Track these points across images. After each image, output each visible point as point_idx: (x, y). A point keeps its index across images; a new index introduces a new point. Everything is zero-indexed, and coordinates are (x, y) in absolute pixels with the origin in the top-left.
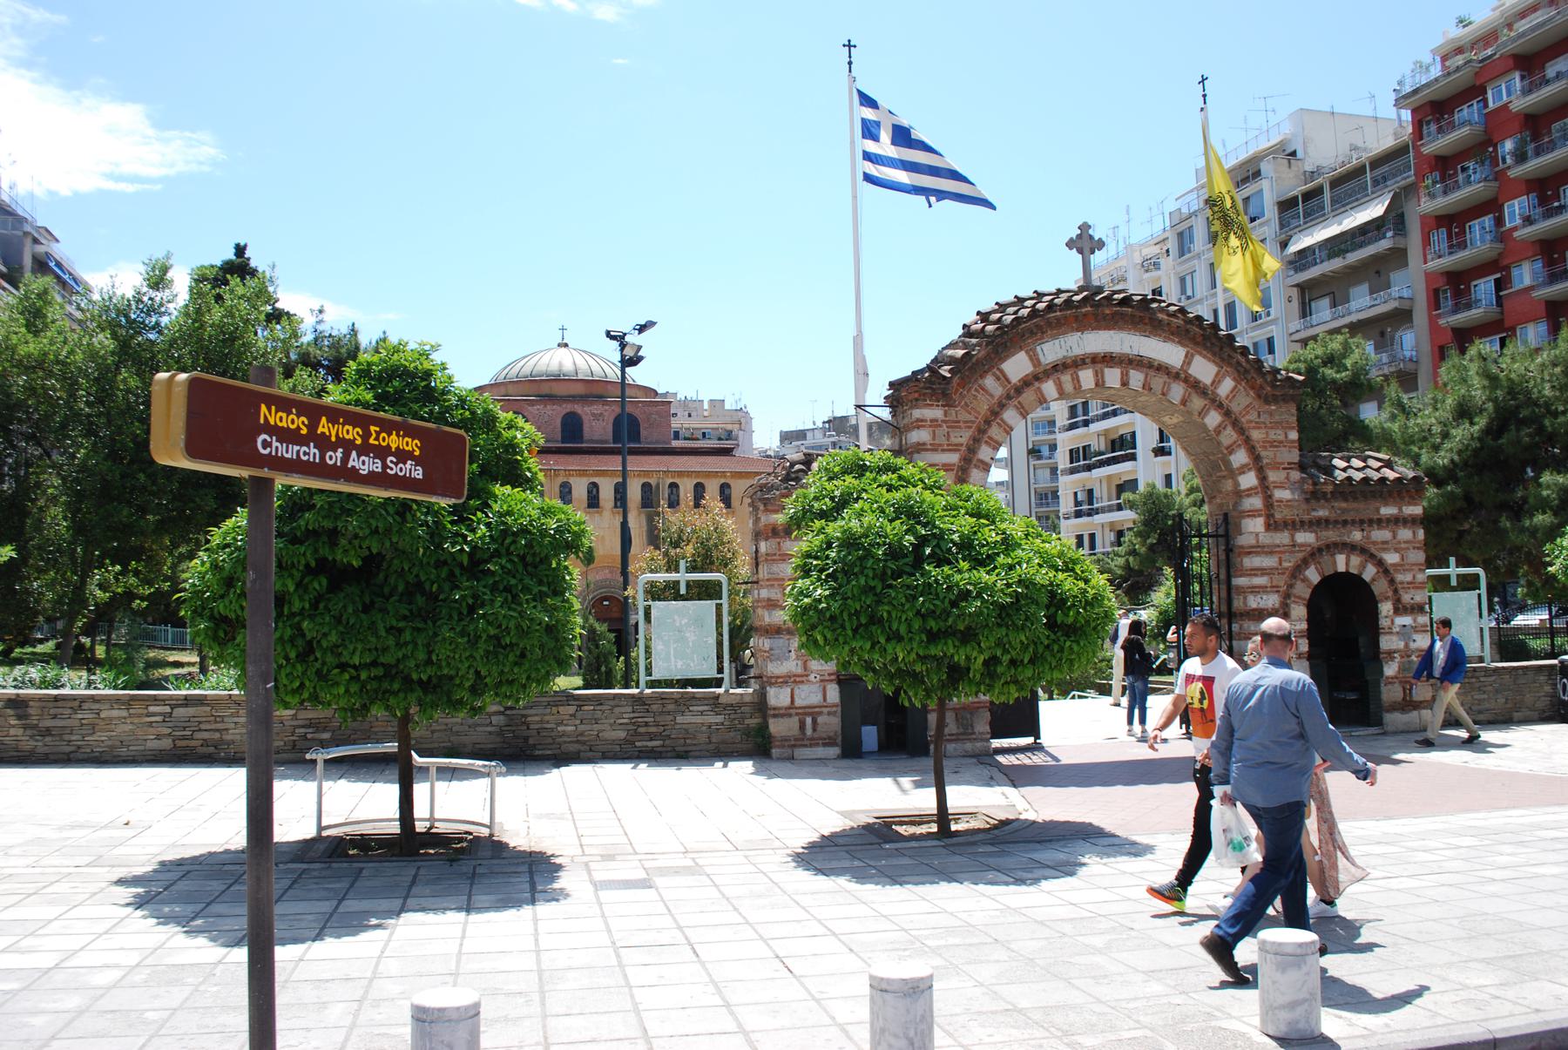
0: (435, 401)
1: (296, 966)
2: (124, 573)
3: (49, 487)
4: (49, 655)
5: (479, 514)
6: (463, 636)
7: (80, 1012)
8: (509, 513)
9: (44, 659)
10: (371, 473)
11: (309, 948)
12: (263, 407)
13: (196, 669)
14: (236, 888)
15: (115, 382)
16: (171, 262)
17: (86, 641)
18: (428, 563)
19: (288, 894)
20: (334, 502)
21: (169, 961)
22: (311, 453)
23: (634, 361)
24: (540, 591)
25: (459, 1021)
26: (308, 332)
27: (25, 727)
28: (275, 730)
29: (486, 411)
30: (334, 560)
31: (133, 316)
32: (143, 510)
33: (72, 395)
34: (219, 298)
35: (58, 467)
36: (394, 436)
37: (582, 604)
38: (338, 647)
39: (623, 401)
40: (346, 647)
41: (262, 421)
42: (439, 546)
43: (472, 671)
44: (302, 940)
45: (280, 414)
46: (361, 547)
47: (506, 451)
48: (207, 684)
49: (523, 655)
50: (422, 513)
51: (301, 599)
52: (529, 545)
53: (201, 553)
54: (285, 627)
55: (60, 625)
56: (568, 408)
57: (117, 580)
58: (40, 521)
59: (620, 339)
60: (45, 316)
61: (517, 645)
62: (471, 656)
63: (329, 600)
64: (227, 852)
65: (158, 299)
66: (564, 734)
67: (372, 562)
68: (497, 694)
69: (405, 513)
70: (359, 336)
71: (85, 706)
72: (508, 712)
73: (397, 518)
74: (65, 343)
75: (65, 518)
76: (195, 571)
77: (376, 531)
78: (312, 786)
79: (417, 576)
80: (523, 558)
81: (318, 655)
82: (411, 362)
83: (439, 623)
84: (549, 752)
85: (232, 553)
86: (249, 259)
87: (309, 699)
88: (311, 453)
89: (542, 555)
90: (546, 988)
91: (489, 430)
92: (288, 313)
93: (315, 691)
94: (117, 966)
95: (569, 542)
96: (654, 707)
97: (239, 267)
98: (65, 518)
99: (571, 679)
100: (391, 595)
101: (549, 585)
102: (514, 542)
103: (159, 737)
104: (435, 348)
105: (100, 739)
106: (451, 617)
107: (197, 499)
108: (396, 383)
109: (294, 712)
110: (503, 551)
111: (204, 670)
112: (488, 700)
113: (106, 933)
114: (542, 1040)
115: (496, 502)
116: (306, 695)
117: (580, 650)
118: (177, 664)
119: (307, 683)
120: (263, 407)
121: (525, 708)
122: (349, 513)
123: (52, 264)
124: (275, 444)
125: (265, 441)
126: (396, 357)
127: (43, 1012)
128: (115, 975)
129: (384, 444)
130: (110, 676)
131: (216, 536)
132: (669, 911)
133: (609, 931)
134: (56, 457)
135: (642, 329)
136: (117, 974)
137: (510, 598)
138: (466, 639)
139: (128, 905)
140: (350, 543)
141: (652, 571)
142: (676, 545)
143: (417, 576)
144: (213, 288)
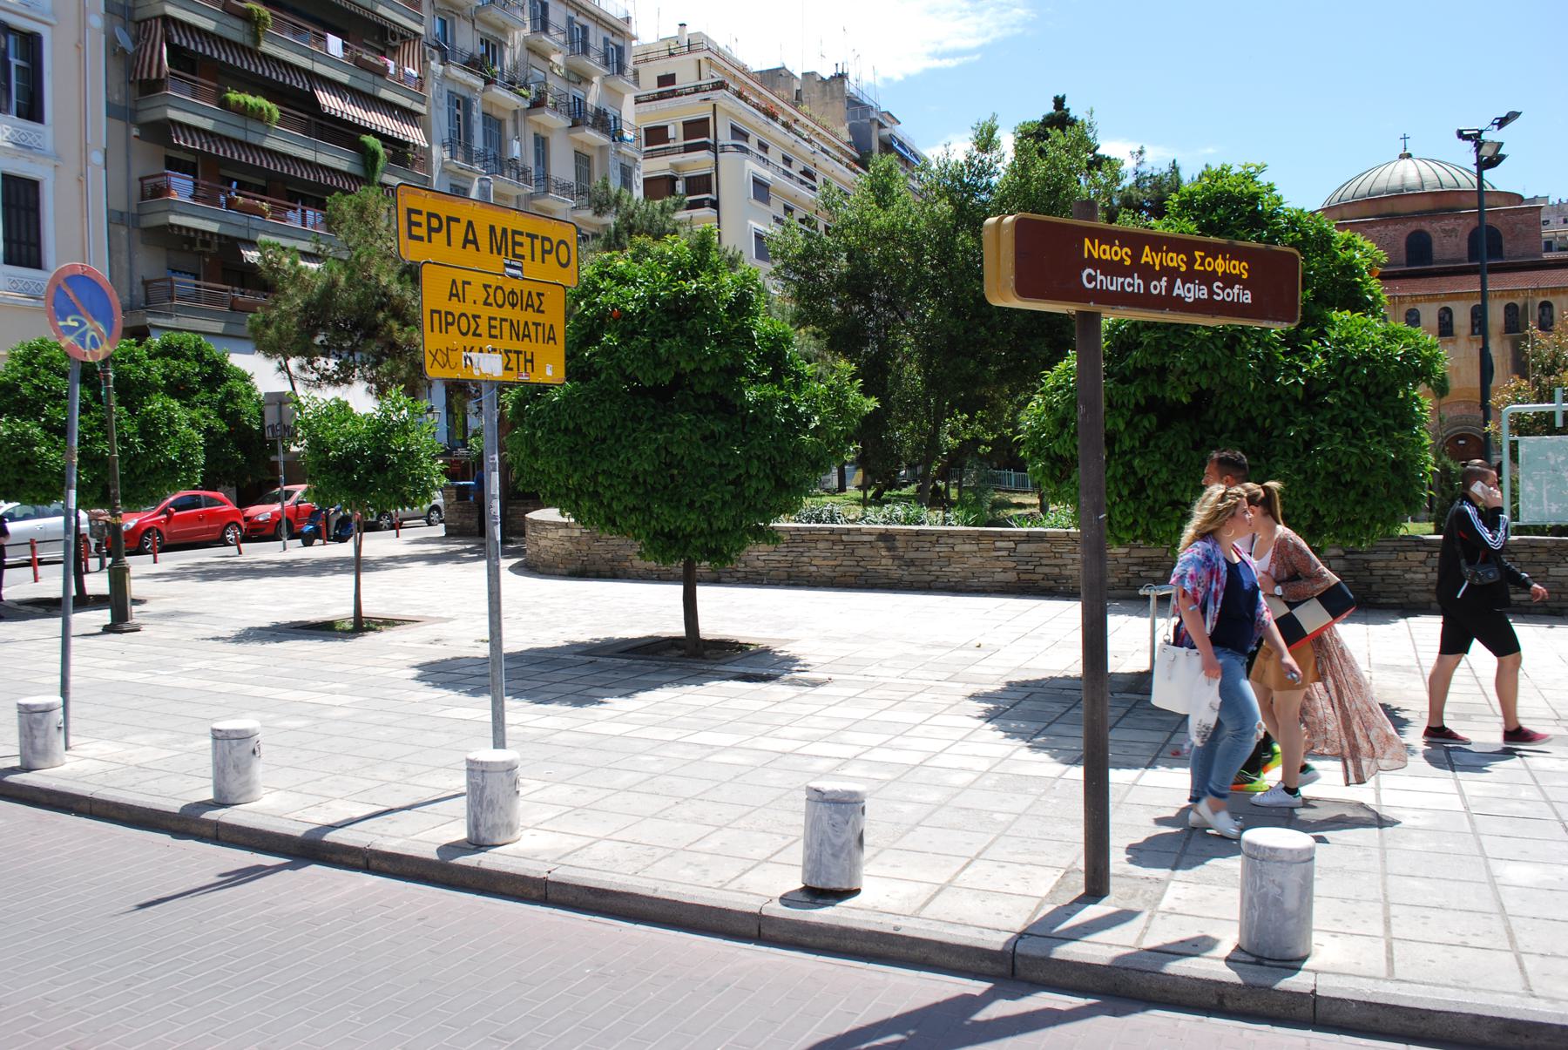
0: (1264, 226)
1: (1129, 790)
2: (971, 420)
3: (904, 346)
4: (912, 497)
5: (1315, 343)
6: (1299, 474)
7: (941, 806)
8: (1349, 340)
9: (907, 499)
10: (1197, 300)
11: (1142, 774)
12: (1087, 242)
13: (1036, 510)
14: (1075, 711)
15: (955, 244)
16: (996, 123)
17: (941, 484)
18: (1260, 398)
19: (1123, 722)
20: (1160, 338)
21: (1015, 771)
22: (1135, 283)
23: (1494, 161)
24: (1385, 424)
25: (1291, 863)
26: (1130, 175)
27: (894, 558)
28: (1109, 567)
29: (1320, 231)
30: (1163, 397)
31: (966, 180)
32: (984, 363)
33: (919, 260)
34: (1042, 152)
35: (909, 327)
36: (1220, 261)
37: (1435, 438)
38: (1169, 484)
39: (1481, 213)
40: (1177, 485)
41: (1086, 255)
42: (1271, 380)
43: (1309, 510)
44: (1136, 767)
45: (1103, 247)
46: (1190, 383)
47: (1344, 273)
48: (1047, 522)
49: (1365, 494)
50: (1252, 345)
51: (1131, 438)
52: (1371, 374)
53: (1036, 396)
54: (1117, 465)
55: (920, 470)
56: (1413, 226)
57: (965, 427)
58: (899, 377)
59: (1476, 138)
60: (892, 191)
61: (1359, 482)
62: (1308, 494)
63: (1159, 438)
64: (1067, 678)
65: (987, 161)
66: (1412, 582)
67: (1201, 398)
68: (1337, 535)
69: (1234, 345)
70: (1181, 173)
71: (942, 540)
72: (1349, 557)
73: (1227, 352)
74: (910, 212)
75: (919, 373)
76: (1032, 414)
77: (1204, 367)
78: (1146, 622)
79: (1248, 411)
80: (1364, 389)
81: (1150, 492)
82: (1236, 187)
83: (1273, 460)
84: (1395, 601)
85: (1065, 394)
86: (1068, 110)
87: (1142, 537)
88: (1135, 283)
89: (1388, 384)
90: (1387, 845)
91: (1323, 252)
92: (1108, 159)
93: (1148, 528)
94: (970, 770)
95: (1420, 369)
96: (1522, 556)
97: (1060, 118)
98: (919, 373)
99: (1421, 525)
100: (1222, 431)
101: (1395, 417)
102: (1355, 372)
103: (1005, 570)
104: (1261, 169)
105: (955, 570)
106: (1285, 454)
107: (1032, 348)
108: (1220, 211)
109: (1127, 550)
110: (1342, 382)
111: (1044, 509)
112: (1327, 541)
113: (961, 740)
114: (1382, 897)
115: (1333, 329)
116: (1139, 532)
117: (1431, 488)
118: (1020, 506)
119: (1140, 520)
120: (1087, 242)
121: (1368, 553)
122: (1177, 348)
123: (895, 145)
124: (1100, 277)
125: (1089, 275)
126: (1219, 183)
127: (910, 801)
128: (968, 777)
129: (1210, 269)
130: (962, 514)
131: (1050, 379)
132: (1536, 782)
133: (1462, 795)
134: (909, 319)
135: (1502, 122)
136: (970, 777)
137: (1350, 432)
138: (1302, 477)
139: (980, 717)
140: (1178, 379)
141: (1518, 402)
142: (1549, 371)
143: (1248, 411)
144: (1036, 142)
